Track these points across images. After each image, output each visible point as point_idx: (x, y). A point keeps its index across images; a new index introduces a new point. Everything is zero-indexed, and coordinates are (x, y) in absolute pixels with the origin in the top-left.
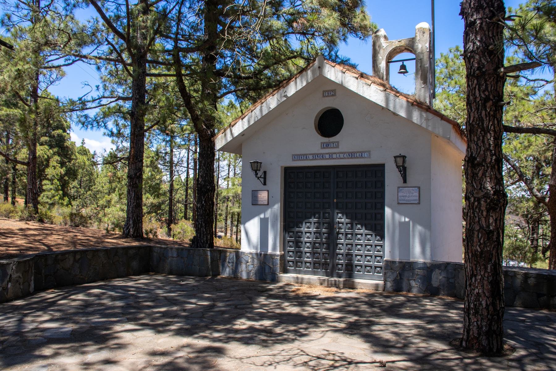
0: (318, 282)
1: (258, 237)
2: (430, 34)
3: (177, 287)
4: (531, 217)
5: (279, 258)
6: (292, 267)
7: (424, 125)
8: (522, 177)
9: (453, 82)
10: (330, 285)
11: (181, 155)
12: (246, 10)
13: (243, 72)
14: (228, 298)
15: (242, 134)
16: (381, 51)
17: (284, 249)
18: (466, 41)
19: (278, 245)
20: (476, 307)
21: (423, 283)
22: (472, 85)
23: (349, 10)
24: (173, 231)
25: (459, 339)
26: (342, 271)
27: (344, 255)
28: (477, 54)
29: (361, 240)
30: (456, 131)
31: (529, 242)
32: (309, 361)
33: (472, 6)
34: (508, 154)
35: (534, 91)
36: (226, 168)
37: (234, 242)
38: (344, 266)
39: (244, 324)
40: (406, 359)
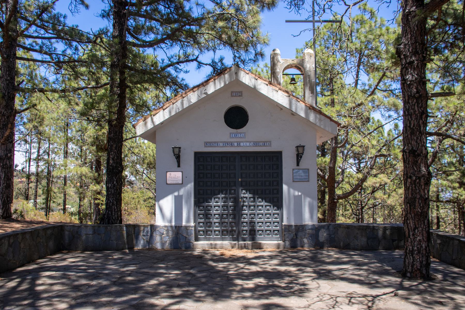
1: (172, 207)
7: (318, 124)
27: (248, 223)
38: (248, 231)
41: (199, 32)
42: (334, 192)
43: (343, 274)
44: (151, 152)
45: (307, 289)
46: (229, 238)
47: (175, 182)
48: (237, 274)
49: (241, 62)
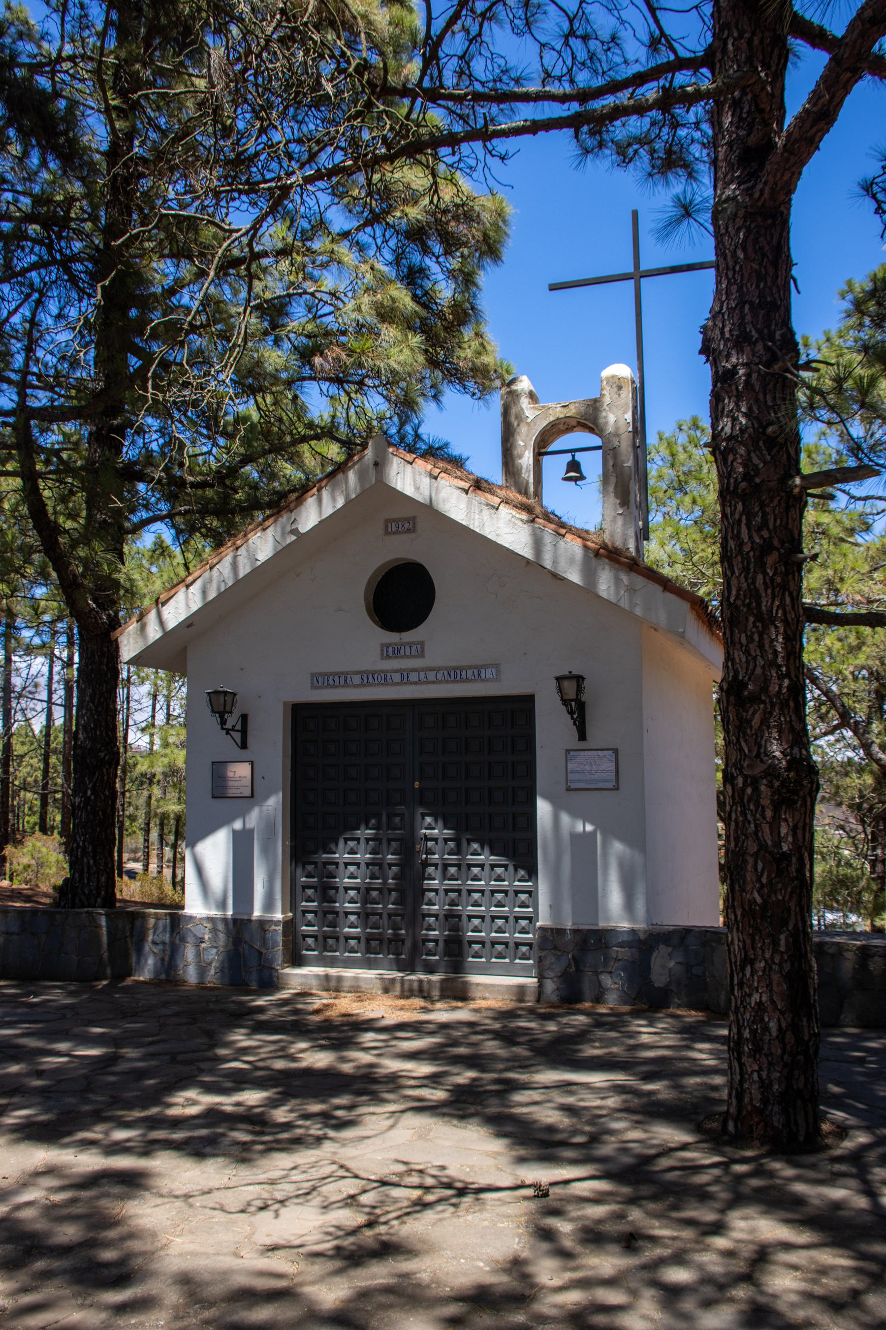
0: (378, 984)
1: (227, 863)
2: (634, 390)
3: (19, 1011)
4: (871, 809)
5: (280, 928)
6: (314, 950)
7: (624, 604)
8: (845, 717)
9: (688, 499)
10: (407, 993)
11: (33, 671)
12: (198, 323)
13: (191, 472)
14: (153, 1036)
15: (188, 624)
16: (523, 429)
17: (293, 907)
18: (716, 414)
19: (278, 896)
20: (755, 1037)
22: (733, 513)
23: (446, 329)
24: (11, 864)
25: (720, 1114)
26: (437, 958)
27: (441, 917)
28: (741, 443)
29: (480, 880)
30: (699, 617)
31: (867, 866)
32: (360, 1194)
33: (727, 335)
34: (814, 665)
35: (865, 523)
36: (147, 702)
37: (168, 888)
38: (441, 944)
39: (194, 1103)
40: (597, 1173)
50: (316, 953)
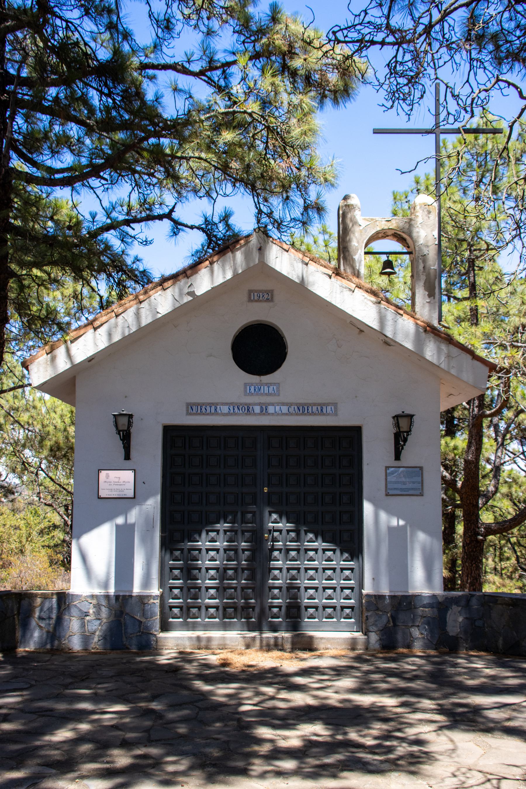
1: (110, 550)
6: (179, 618)
21: (431, 631)
26: (280, 620)
27: (284, 589)
29: (314, 560)
38: (283, 609)
41: (179, 154)
42: (478, 516)
43: (509, 719)
44: (59, 421)
45: (426, 753)
46: (238, 625)
47: (114, 494)
48: (261, 714)
49: (273, 224)
50: (181, 620)
